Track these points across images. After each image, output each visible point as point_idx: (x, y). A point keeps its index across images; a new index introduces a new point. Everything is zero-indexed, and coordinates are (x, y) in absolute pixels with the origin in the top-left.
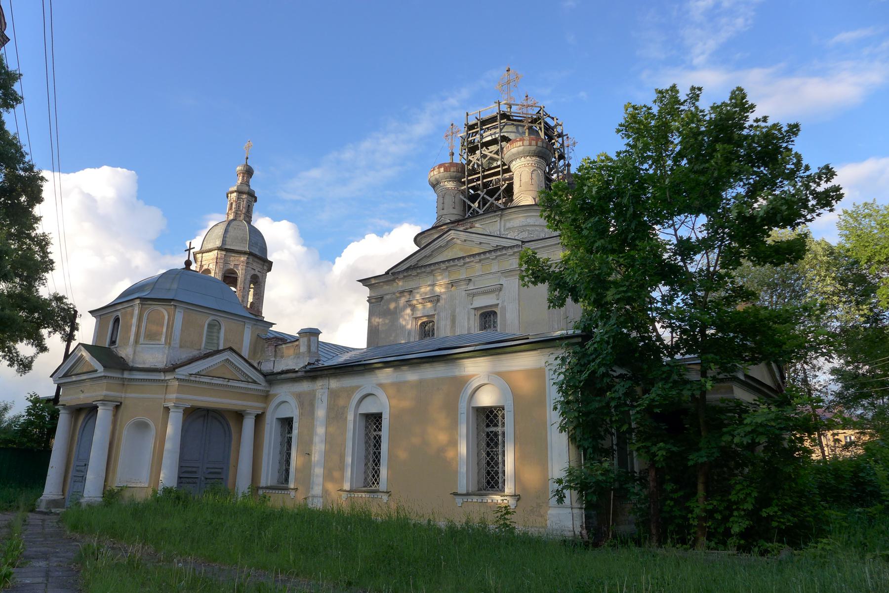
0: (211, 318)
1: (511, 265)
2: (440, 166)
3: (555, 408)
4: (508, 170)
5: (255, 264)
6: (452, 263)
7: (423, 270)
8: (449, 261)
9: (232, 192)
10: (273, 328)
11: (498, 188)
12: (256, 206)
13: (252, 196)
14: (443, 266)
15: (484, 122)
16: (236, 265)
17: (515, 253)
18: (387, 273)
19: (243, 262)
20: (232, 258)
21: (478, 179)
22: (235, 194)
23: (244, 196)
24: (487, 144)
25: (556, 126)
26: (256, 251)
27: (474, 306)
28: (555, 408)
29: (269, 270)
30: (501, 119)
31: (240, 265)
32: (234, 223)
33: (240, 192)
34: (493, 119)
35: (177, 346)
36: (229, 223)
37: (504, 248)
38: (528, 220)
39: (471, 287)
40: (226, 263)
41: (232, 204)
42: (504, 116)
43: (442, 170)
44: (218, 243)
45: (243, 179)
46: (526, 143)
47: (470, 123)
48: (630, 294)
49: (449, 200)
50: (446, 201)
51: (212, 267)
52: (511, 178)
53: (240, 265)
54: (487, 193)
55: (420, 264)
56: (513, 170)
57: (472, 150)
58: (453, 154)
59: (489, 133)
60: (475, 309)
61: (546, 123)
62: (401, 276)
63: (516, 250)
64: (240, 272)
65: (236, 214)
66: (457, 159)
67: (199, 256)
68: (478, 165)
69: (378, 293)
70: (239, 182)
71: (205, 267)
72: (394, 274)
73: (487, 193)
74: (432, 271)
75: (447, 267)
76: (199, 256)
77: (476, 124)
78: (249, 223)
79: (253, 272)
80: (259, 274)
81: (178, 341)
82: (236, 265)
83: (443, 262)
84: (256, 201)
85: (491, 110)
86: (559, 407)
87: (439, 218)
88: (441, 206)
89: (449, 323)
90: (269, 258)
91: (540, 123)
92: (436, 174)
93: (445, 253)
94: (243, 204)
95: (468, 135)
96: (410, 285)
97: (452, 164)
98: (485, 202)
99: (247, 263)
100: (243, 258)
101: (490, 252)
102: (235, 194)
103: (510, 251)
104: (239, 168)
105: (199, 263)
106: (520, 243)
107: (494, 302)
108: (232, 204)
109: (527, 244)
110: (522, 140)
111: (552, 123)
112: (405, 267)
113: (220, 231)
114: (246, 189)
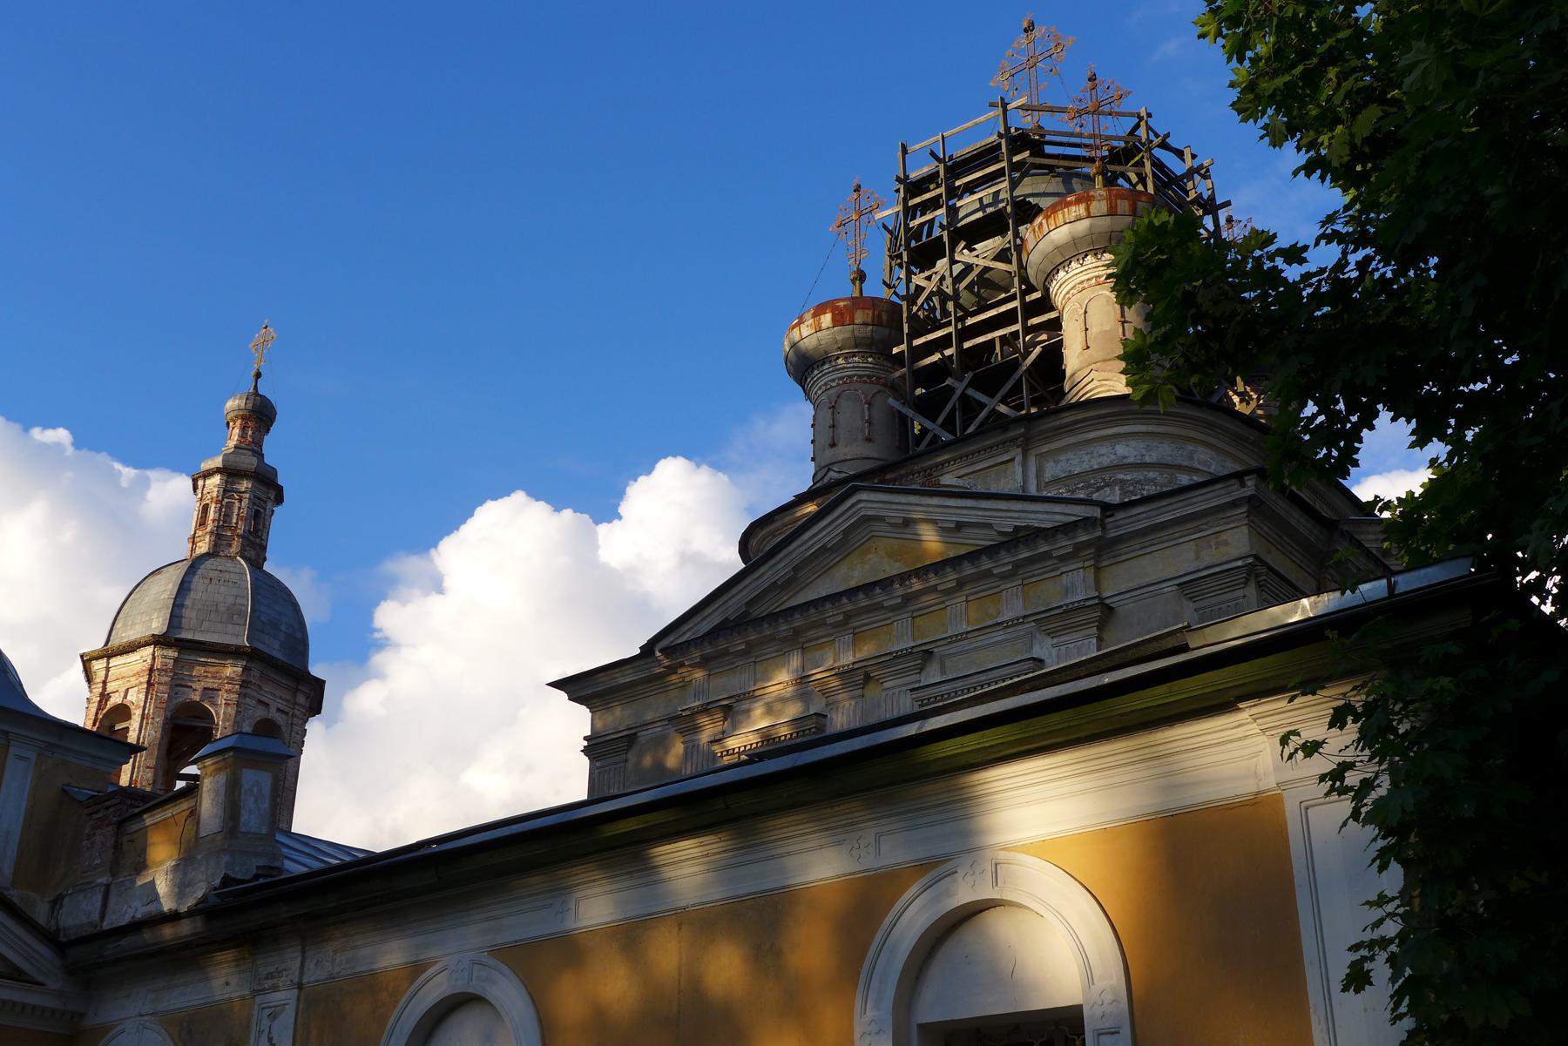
2: (819, 310)
3: (1358, 979)
4: (1045, 304)
5: (267, 688)
6: (863, 600)
7: (768, 631)
8: (851, 593)
9: (208, 474)
11: (1016, 364)
12: (280, 520)
13: (268, 487)
14: (832, 614)
15: (957, 168)
16: (210, 693)
17: (1079, 548)
18: (647, 650)
19: (230, 680)
20: (198, 671)
21: (945, 342)
22: (216, 480)
23: (245, 485)
24: (973, 234)
25: (1191, 173)
26: (274, 649)
28: (1358, 979)
29: (315, 708)
30: (1013, 151)
31: (222, 692)
32: (210, 563)
33: (230, 472)
34: (988, 155)
36: (195, 564)
38: (1121, 449)
39: (932, 675)
40: (178, 683)
41: (205, 509)
42: (1020, 141)
43: (826, 319)
44: (158, 625)
45: (243, 435)
46: (1099, 207)
47: (914, 175)
49: (851, 416)
50: (842, 419)
51: (136, 698)
52: (1055, 325)
53: (222, 692)
54: (973, 384)
55: (758, 611)
56: (1058, 301)
57: (924, 255)
58: (861, 277)
59: (968, 199)
61: (1158, 165)
62: (696, 655)
63: (1083, 537)
64: (222, 713)
65: (219, 539)
66: (874, 289)
67: (99, 666)
68: (944, 298)
69: (619, 717)
70: (232, 443)
71: (116, 700)
72: (674, 646)
73: (973, 384)
74: (797, 632)
75: (848, 617)
76: (99, 666)
77: (932, 178)
78: (256, 563)
79: (260, 713)
80: (279, 719)
82: (210, 693)
83: (834, 598)
84: (279, 500)
85: (975, 129)
86: (1380, 969)
87: (822, 469)
88: (826, 437)
90: (316, 670)
91: (1140, 164)
92: (812, 332)
93: (842, 570)
94: (241, 508)
95: (910, 212)
96: (723, 686)
97: (859, 302)
98: (970, 408)
99: (244, 684)
100: (231, 670)
101: (990, 551)
102: (216, 480)
103: (1064, 544)
104: (232, 404)
105: (98, 689)
106: (1096, 512)
108: (205, 509)
109: (1120, 515)
110: (1086, 199)
111: (1178, 167)
112: (705, 627)
113: (165, 588)
114: (249, 462)
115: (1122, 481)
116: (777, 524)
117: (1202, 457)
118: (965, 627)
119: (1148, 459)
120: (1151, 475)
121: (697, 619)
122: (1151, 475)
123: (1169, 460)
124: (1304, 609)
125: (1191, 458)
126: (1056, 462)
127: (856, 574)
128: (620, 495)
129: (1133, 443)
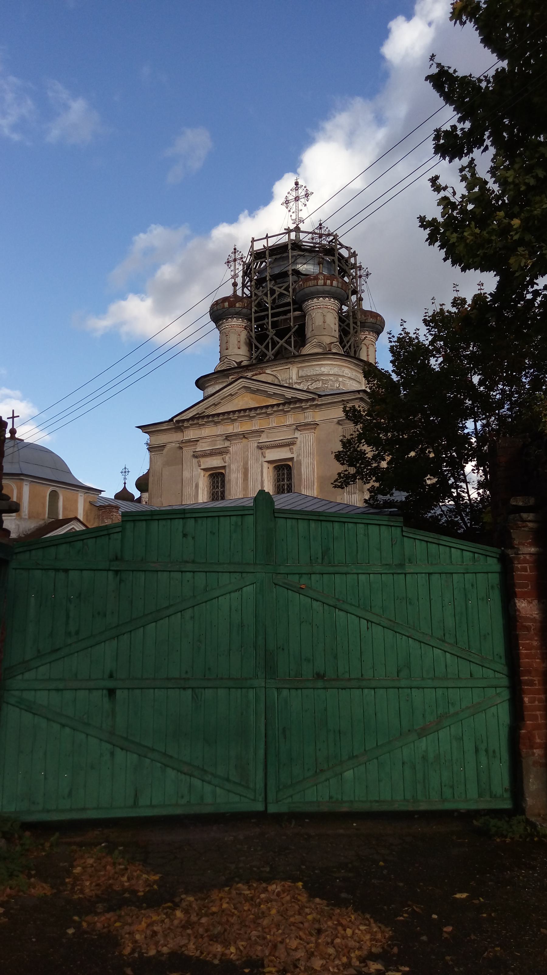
0: (51, 489)
1: (307, 417)
10: (103, 495)
18: (171, 420)
27: (267, 459)
35: (27, 517)
37: (300, 401)
48: (110, 882)
60: (269, 462)
81: (27, 512)
89: (240, 475)
93: (236, 401)
107: (289, 455)
112: (191, 415)
115: (323, 379)
116: (210, 377)
117: (347, 372)
118: (275, 425)
119: (331, 373)
120: (331, 378)
121: (188, 412)
122: (331, 378)
123: (337, 373)
124: (32, 600)
125: (343, 372)
126: (303, 371)
127: (241, 403)
128: (413, 8)
129: (326, 367)
